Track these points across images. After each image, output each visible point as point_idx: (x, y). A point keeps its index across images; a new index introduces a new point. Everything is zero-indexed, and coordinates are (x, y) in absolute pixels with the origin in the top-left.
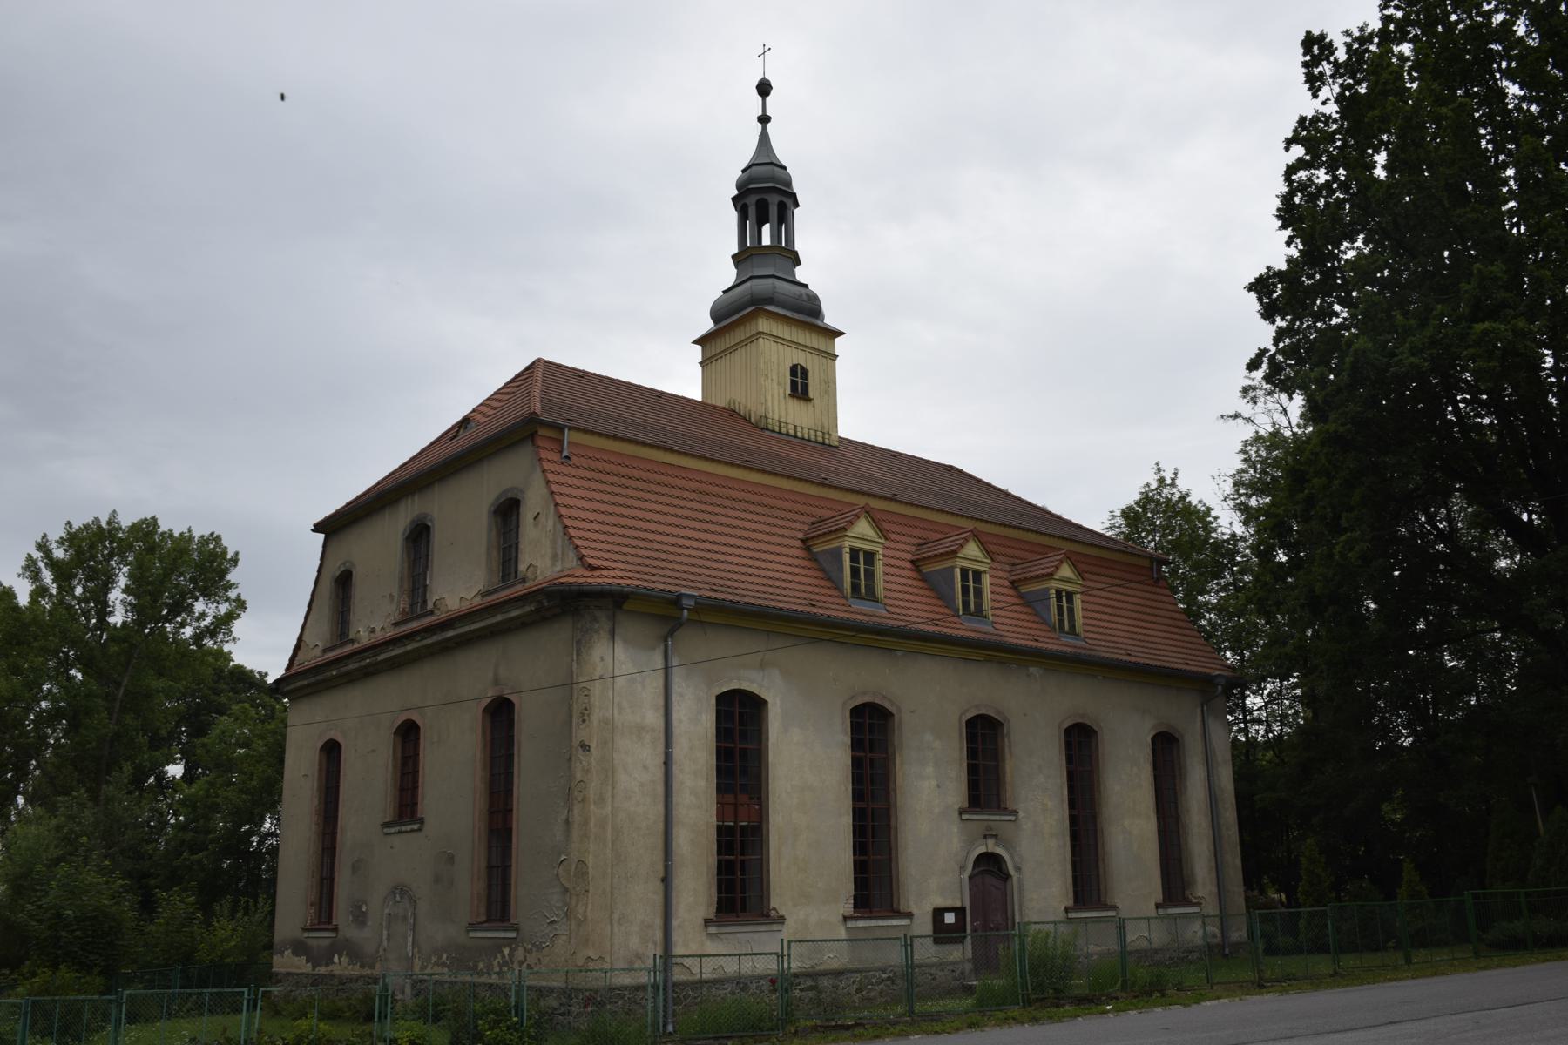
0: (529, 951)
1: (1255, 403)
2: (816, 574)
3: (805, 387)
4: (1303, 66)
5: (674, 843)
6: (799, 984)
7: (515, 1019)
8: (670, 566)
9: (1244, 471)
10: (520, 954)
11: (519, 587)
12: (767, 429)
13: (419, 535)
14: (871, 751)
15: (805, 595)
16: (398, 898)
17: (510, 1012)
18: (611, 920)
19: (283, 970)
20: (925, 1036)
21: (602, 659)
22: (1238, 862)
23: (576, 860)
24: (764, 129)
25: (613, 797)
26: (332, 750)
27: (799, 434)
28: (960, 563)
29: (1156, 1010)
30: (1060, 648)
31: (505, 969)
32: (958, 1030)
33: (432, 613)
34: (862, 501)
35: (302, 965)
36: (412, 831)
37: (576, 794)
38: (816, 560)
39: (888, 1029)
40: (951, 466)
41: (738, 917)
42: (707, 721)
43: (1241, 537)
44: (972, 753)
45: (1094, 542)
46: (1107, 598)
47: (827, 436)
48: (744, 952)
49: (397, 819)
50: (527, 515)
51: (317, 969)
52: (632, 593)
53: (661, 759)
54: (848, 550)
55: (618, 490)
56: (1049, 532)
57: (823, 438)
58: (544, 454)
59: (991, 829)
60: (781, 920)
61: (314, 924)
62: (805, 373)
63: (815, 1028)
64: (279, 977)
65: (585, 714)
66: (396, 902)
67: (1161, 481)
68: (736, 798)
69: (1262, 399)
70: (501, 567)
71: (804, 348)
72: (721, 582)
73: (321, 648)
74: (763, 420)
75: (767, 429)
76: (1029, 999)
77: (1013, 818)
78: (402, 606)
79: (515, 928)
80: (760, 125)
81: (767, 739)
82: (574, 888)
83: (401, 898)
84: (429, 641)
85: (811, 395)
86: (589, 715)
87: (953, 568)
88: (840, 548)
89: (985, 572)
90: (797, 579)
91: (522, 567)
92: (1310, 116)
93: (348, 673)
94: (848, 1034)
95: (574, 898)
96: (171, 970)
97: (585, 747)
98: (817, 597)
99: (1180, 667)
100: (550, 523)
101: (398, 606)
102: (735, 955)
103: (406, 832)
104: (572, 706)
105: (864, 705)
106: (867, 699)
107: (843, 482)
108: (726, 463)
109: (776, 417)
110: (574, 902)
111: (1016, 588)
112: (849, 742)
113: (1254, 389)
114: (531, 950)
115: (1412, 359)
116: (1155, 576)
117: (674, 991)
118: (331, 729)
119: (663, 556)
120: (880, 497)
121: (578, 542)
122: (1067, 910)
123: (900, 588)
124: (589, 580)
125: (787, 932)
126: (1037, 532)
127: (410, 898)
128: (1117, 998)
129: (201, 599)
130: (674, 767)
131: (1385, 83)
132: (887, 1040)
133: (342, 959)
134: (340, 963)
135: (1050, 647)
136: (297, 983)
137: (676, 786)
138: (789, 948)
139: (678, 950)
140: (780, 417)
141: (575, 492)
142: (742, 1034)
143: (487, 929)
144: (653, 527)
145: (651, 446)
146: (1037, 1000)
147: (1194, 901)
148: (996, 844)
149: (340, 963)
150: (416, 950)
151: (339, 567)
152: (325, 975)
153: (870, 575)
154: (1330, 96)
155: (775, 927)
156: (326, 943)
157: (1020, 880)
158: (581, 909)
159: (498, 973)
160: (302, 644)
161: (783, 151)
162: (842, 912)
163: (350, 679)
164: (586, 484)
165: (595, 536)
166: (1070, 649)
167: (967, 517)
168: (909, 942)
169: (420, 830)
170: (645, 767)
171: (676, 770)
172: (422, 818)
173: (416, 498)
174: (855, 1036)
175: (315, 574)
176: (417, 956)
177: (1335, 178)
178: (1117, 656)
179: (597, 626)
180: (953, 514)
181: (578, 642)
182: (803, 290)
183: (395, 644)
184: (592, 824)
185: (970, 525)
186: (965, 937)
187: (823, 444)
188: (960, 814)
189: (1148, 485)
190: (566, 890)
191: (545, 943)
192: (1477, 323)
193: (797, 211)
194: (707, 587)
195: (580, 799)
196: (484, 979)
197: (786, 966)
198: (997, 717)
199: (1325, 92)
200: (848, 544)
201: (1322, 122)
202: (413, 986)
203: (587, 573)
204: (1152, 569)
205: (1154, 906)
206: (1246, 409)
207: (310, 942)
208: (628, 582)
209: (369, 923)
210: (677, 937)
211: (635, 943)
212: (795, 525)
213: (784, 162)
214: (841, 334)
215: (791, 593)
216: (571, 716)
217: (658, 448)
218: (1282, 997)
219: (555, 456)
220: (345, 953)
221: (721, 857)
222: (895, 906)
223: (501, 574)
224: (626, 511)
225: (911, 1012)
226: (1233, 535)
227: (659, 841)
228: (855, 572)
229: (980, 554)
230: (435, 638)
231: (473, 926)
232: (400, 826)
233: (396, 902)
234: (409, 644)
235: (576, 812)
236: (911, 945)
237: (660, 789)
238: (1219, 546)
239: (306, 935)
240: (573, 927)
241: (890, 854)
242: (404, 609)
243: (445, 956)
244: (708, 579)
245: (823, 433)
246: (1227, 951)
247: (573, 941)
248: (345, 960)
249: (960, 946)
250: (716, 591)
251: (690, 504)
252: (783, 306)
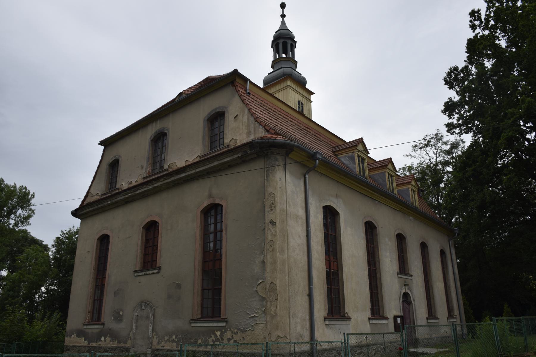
10: (229, 334)
16: (143, 307)
18: (289, 316)
19: (71, 344)
21: (280, 179)
23: (269, 282)
24: (283, 20)
25: (288, 249)
35: (82, 342)
36: (153, 273)
37: (268, 247)
42: (320, 217)
48: (386, 332)
49: (142, 269)
50: (229, 118)
51: (90, 344)
53: (305, 234)
61: (90, 322)
62: (302, 104)
64: (68, 348)
65: (272, 207)
70: (210, 145)
78: (148, 170)
79: (225, 320)
81: (340, 231)
82: (269, 298)
83: (145, 307)
84: (169, 181)
86: (274, 207)
93: (116, 202)
95: (269, 304)
96: (12, 344)
97: (273, 223)
100: (245, 119)
103: (149, 274)
110: (268, 306)
114: (237, 332)
118: (104, 230)
127: (151, 307)
129: (20, 209)
133: (107, 339)
134: (105, 341)
136: (79, 350)
149: (105, 341)
150: (155, 333)
151: (112, 159)
152: (96, 347)
156: (98, 330)
158: (273, 309)
159: (212, 345)
160: (89, 194)
161: (290, 26)
163: (117, 205)
169: (158, 273)
173: (158, 122)
175: (100, 158)
176: (155, 337)
179: (277, 163)
181: (268, 171)
188: (398, 274)
190: (264, 299)
191: (247, 328)
195: (270, 250)
196: (201, 349)
198: (404, 235)
205: (446, 318)
207: (87, 330)
214: (313, 93)
216: (264, 207)
220: (108, 336)
222: (381, 314)
223: (210, 148)
227: (306, 275)
230: (172, 179)
231: (193, 321)
232: (145, 271)
234: (156, 183)
235: (269, 256)
239: (85, 327)
240: (268, 319)
242: (149, 171)
243: (174, 337)
247: (268, 327)
248: (108, 339)
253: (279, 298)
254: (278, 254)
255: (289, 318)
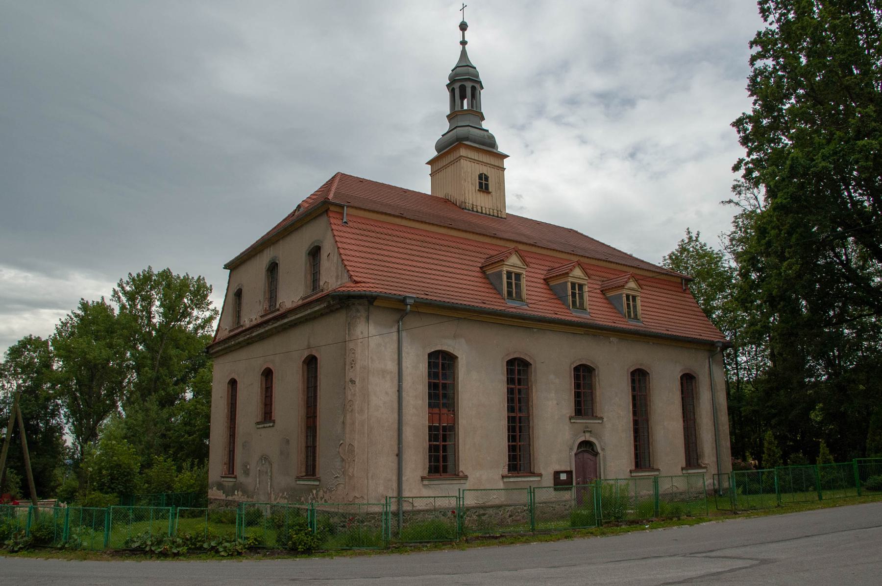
0: (325, 492)
1: (740, 194)
2: (488, 286)
3: (487, 185)
4: (758, 4)
5: (403, 435)
6: (476, 512)
7: (310, 529)
8: (402, 281)
9: (735, 232)
10: (321, 493)
11: (320, 294)
12: (466, 209)
13: (273, 268)
14: (518, 385)
15: (480, 298)
16: (263, 462)
17: (307, 525)
18: (367, 477)
19: (212, 497)
20: (540, 543)
22: (728, 444)
24: (464, 48)
25: (368, 409)
26: (233, 383)
27: (484, 212)
28: (570, 280)
29: (674, 528)
30: (628, 327)
31: (314, 501)
32: (559, 539)
33: (278, 310)
34: (512, 245)
35: (219, 495)
36: (270, 427)
38: (488, 279)
39: (519, 538)
40: (571, 229)
41: (441, 475)
42: (423, 367)
43: (734, 269)
44: (577, 386)
45: (649, 269)
46: (657, 300)
47: (499, 212)
52: (378, 296)
54: (505, 272)
55: (375, 240)
56: (623, 263)
57: (498, 214)
58: (332, 221)
59: (588, 428)
60: (466, 477)
62: (487, 179)
63: (477, 538)
65: (353, 363)
66: (263, 464)
67: (690, 238)
68: (440, 410)
69: (744, 192)
71: (486, 164)
72: (431, 290)
73: (228, 330)
74: (463, 204)
75: (466, 209)
76: (601, 522)
77: (600, 421)
80: (461, 46)
85: (490, 190)
87: (566, 282)
88: (501, 272)
89: (585, 284)
90: (476, 288)
91: (321, 283)
92: (763, 32)
93: (239, 343)
94: (497, 541)
97: (353, 382)
98: (487, 299)
99: (696, 337)
100: (336, 258)
101: (263, 307)
102: (432, 497)
104: (345, 359)
105: (515, 359)
106: (516, 356)
107: (506, 236)
108: (437, 225)
109: (471, 203)
111: (604, 294)
112: (506, 380)
113: (740, 186)
115: (823, 164)
116: (684, 288)
117: (403, 516)
119: (398, 276)
120: (526, 244)
121: (349, 268)
122: (631, 472)
123: (536, 294)
124: (354, 289)
125: (468, 485)
126: (617, 263)
128: (652, 521)
130: (403, 393)
131: (804, 8)
132: (518, 545)
135: (622, 326)
137: (404, 403)
138: (463, 493)
139: (406, 494)
140: (473, 202)
141: (348, 241)
142: (436, 540)
143: (304, 480)
144: (394, 260)
145: (394, 216)
146: (606, 522)
147: (703, 466)
148: (590, 436)
153: (518, 286)
154: (774, 20)
155: (462, 481)
156: (231, 484)
157: (604, 457)
158: (351, 470)
161: (473, 60)
162: (501, 473)
163: (241, 346)
164: (356, 237)
165: (359, 265)
166: (633, 327)
167: (577, 255)
168: (532, 491)
169: (273, 426)
170: (387, 393)
171: (404, 394)
172: (274, 420)
174: (500, 542)
177: (778, 63)
178: (660, 331)
179: (359, 314)
180: (568, 253)
181: (349, 324)
182: (485, 133)
183: (260, 327)
184: (357, 424)
185: (575, 259)
186: (572, 488)
187: (498, 217)
188: (570, 419)
189: (683, 241)
190: (343, 460)
192: (859, 140)
193: (482, 91)
194: (423, 293)
195: (350, 410)
196: (303, 507)
197: (461, 503)
199: (771, 18)
200: (505, 269)
201: (770, 34)
202: (271, 508)
203: (353, 285)
204: (682, 284)
206: (736, 198)
208: (376, 290)
209: (251, 475)
210: (405, 486)
211: (381, 489)
212: (477, 259)
213: (474, 65)
215: (471, 296)
216: (345, 364)
217: (397, 217)
218: (746, 520)
219: (340, 222)
221: (431, 443)
222: (532, 470)
224: (378, 252)
225: (533, 530)
226: (730, 268)
228: (509, 284)
229: (582, 275)
230: (279, 323)
231: (298, 478)
233: (263, 464)
235: (348, 417)
236: (534, 493)
237: (396, 405)
238: (721, 274)
239: (223, 479)
240: (347, 480)
241: (530, 442)
243: (285, 493)
244: (423, 289)
245: (498, 211)
246: (721, 493)
249: (569, 492)
250: (427, 295)
251: (415, 248)
252: (475, 142)
253: (356, 460)
254: (357, 414)
255: (368, 479)
